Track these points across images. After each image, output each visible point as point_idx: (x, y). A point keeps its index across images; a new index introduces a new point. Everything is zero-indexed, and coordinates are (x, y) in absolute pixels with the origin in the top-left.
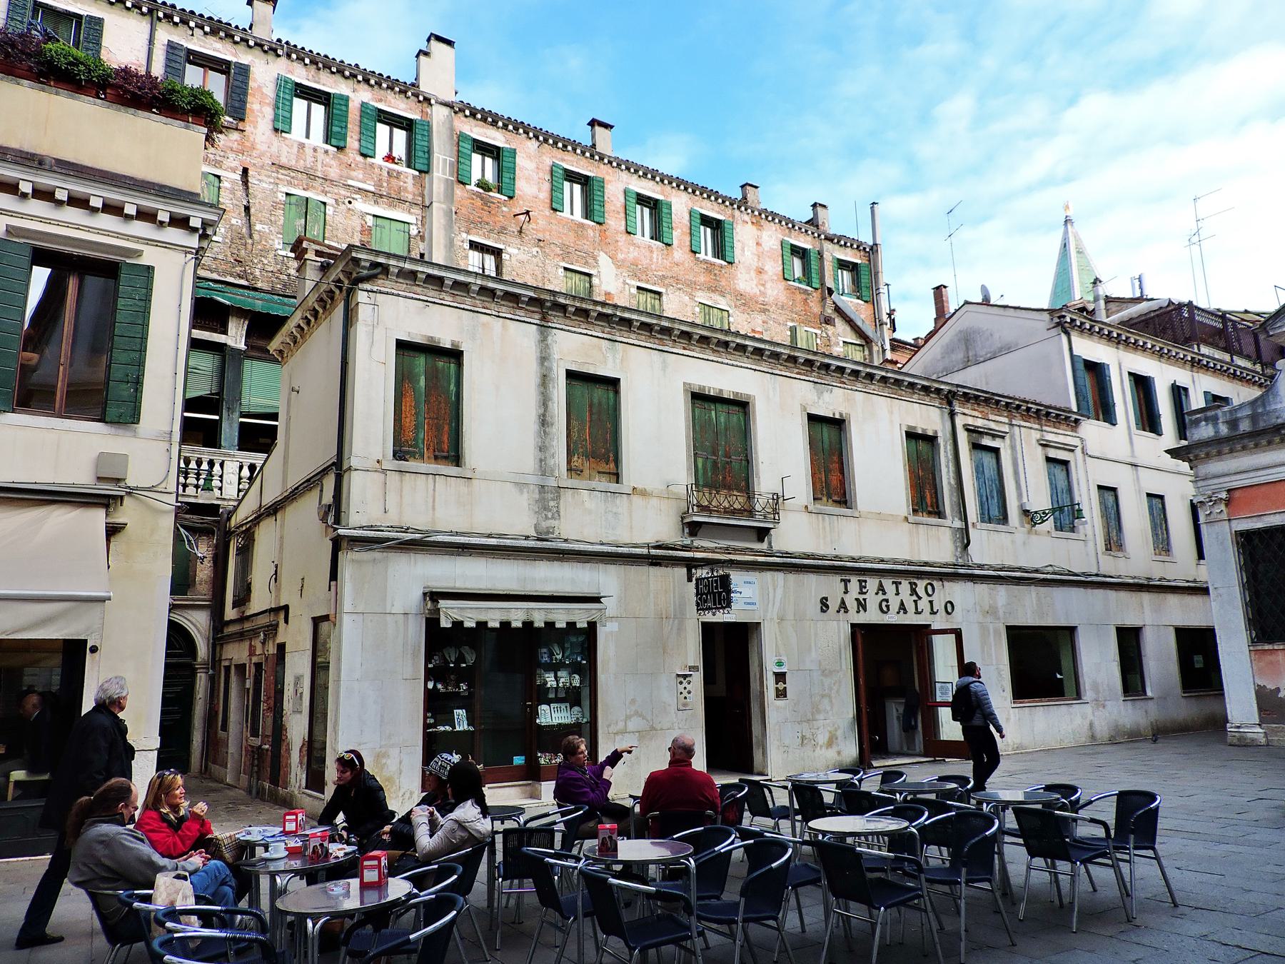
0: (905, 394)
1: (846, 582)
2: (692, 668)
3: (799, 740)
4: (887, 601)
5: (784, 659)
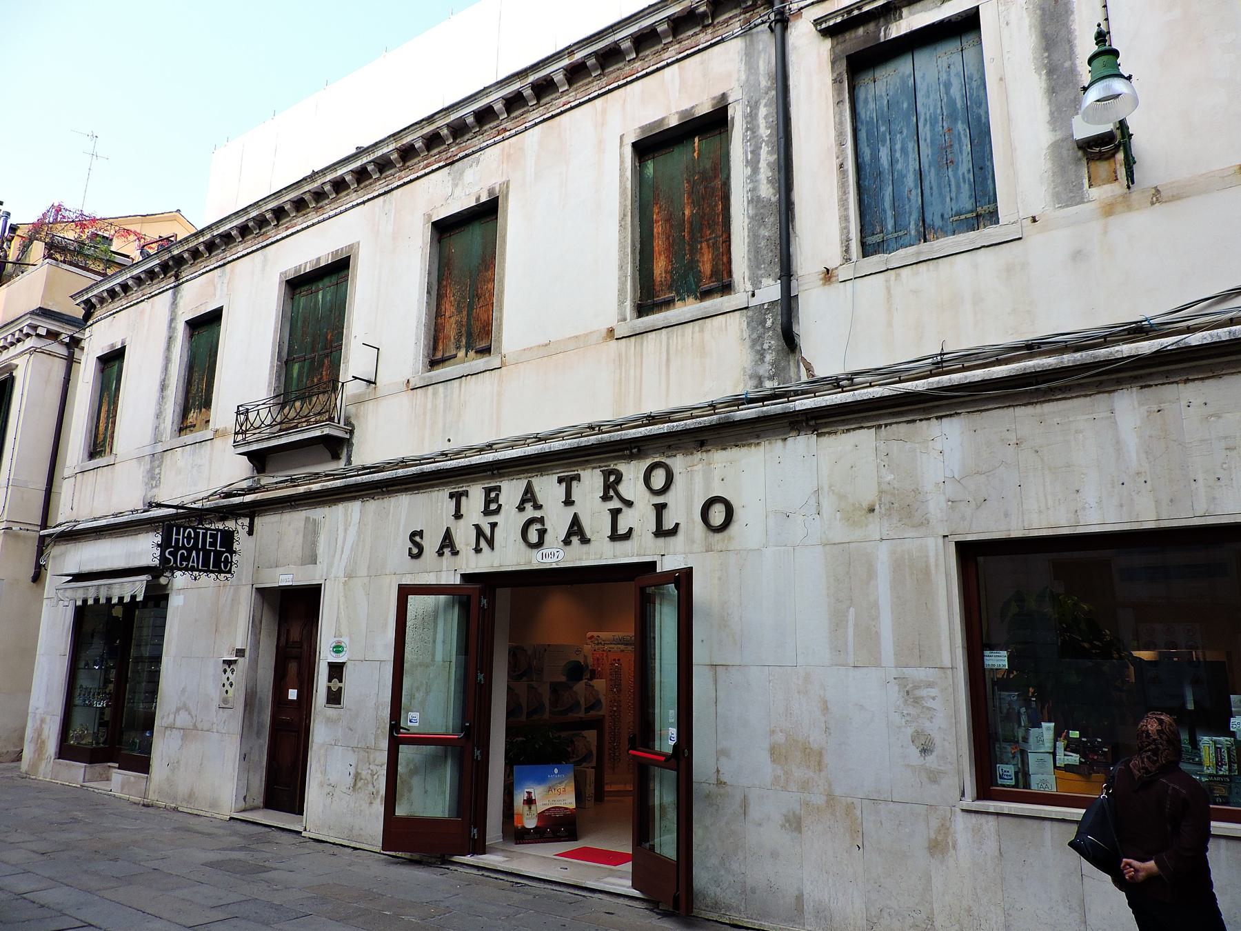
0: (273, 233)
1: (457, 497)
2: (240, 653)
3: (350, 780)
4: (541, 520)
5: (345, 641)
